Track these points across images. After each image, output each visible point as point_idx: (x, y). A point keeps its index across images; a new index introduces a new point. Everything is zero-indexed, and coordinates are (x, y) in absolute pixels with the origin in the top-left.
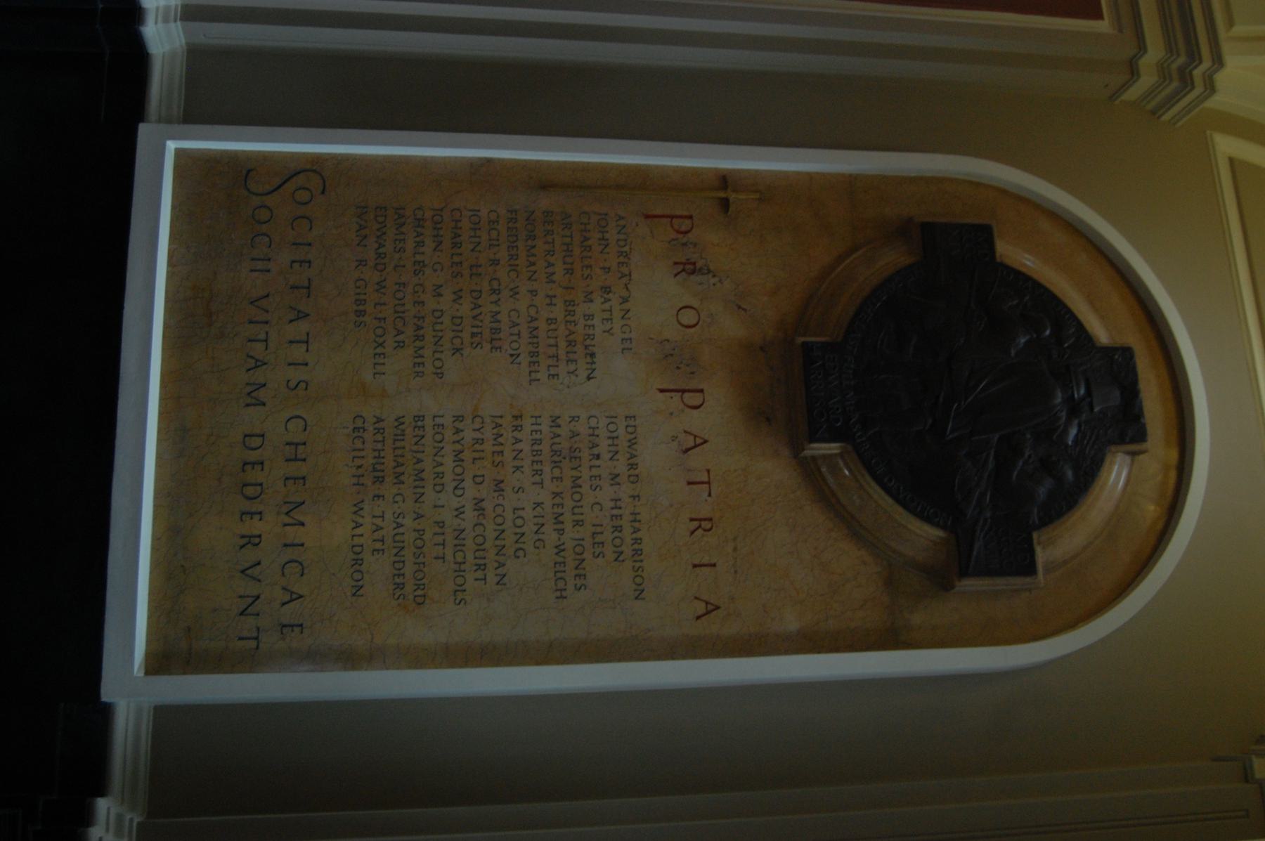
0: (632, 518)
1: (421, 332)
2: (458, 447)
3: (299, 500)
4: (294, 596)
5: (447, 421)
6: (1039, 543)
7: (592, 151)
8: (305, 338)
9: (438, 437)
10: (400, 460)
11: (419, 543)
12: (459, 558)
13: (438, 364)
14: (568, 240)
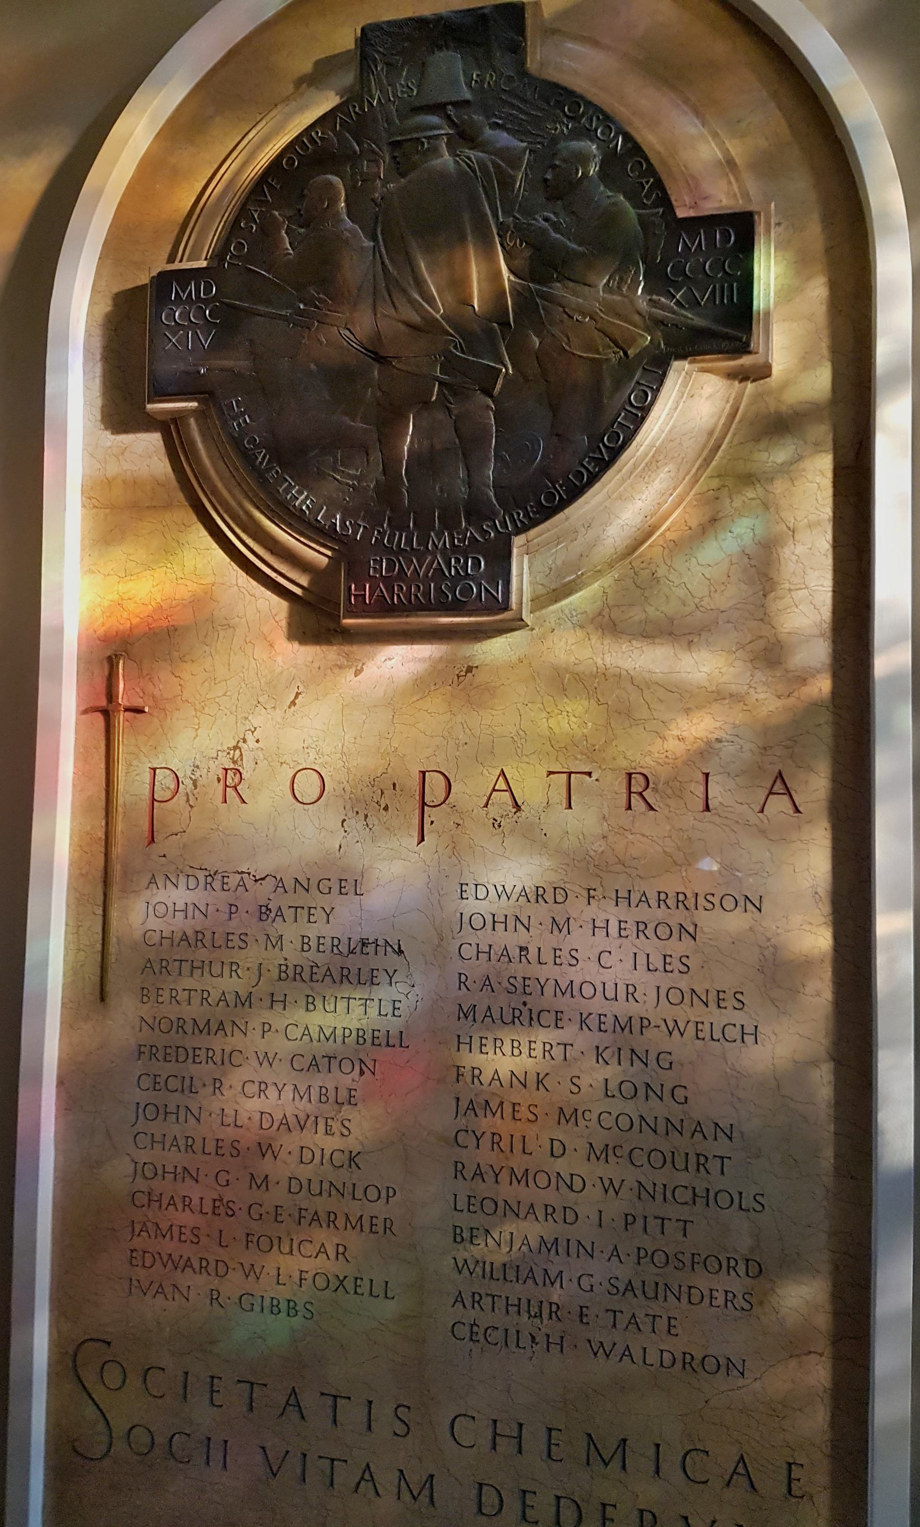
0: (623, 903)
1: (323, 1216)
2: (504, 1176)
3: (584, 1443)
4: (741, 1470)
5: (463, 1189)
6: (695, 206)
7: (46, 932)
8: (329, 1401)
9: (489, 1206)
10: (523, 1274)
11: (659, 1258)
12: (684, 1195)
13: (372, 1194)
14: (186, 967)
